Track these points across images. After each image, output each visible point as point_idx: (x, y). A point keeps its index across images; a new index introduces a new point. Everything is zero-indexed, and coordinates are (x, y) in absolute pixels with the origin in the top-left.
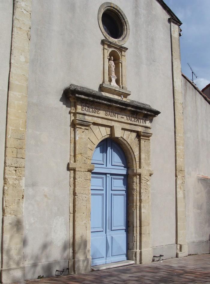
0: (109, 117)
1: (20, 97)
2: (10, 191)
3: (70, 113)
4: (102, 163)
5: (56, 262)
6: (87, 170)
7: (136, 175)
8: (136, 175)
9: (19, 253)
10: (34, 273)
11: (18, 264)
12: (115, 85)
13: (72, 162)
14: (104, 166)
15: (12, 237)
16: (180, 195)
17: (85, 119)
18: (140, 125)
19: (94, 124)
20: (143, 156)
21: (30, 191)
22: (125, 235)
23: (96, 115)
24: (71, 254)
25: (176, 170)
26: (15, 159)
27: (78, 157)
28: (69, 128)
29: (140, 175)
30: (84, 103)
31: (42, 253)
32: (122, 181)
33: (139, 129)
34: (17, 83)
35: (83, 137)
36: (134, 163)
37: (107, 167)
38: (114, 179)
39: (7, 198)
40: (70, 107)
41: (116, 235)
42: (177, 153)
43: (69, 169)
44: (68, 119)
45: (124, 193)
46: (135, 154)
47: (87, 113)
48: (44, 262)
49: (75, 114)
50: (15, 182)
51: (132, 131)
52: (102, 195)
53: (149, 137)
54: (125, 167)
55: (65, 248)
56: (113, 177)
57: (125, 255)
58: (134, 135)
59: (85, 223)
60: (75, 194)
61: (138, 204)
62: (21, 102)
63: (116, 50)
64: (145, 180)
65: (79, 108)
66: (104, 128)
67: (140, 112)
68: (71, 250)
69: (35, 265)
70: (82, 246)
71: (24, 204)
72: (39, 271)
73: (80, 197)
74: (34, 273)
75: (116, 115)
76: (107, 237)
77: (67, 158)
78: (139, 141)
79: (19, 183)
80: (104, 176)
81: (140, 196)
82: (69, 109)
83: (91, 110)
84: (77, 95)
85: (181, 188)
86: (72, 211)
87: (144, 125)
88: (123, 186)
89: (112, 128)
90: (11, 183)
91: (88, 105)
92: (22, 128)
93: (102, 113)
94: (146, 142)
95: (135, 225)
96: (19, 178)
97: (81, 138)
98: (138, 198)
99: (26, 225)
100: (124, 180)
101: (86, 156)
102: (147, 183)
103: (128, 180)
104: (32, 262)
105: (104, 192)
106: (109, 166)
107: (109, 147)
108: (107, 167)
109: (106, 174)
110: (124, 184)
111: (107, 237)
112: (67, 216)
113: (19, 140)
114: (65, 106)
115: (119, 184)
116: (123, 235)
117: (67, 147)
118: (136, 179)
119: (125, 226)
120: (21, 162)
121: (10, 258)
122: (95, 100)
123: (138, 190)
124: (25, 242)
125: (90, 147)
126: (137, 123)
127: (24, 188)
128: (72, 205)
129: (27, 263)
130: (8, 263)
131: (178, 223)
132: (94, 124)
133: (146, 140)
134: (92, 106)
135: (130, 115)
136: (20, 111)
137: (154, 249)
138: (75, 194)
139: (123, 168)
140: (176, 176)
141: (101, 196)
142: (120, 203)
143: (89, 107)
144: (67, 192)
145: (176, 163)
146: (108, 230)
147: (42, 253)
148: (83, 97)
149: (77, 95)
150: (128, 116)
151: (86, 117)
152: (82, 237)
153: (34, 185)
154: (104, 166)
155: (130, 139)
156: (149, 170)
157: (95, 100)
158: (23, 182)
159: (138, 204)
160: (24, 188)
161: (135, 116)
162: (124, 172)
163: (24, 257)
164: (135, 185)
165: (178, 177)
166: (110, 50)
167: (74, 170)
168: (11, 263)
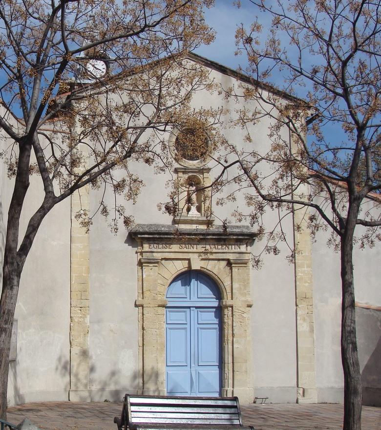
0: (186, 250)
3: (137, 253)
4: (185, 296)
5: (125, 389)
6: (157, 306)
7: (227, 307)
8: (227, 307)
9: (86, 377)
10: (101, 396)
11: (86, 386)
12: (196, 212)
13: (140, 299)
14: (188, 299)
15: (79, 364)
16: (303, 327)
17: (153, 256)
18: (231, 252)
21: (96, 327)
23: (168, 250)
24: (141, 384)
25: (296, 298)
26: (79, 301)
27: (147, 294)
28: (136, 268)
29: (232, 307)
30: (150, 241)
31: (111, 379)
32: (213, 314)
33: (231, 257)
36: (225, 294)
37: (191, 300)
39: (73, 333)
40: (137, 247)
42: (298, 277)
43: (136, 306)
44: (136, 258)
45: (217, 326)
46: (225, 284)
48: (112, 387)
49: (141, 253)
50: (80, 320)
51: (219, 260)
52: (185, 329)
53: (246, 263)
54: (217, 299)
55: (135, 377)
56: (199, 310)
57: (218, 393)
58: (224, 263)
59: (155, 356)
60: (143, 329)
61: (230, 339)
62: (83, 252)
63: (195, 174)
64: (240, 311)
65: (146, 247)
67: (227, 238)
68: (141, 381)
69: (103, 389)
70: (153, 377)
71: (89, 339)
72: (106, 396)
73: (149, 332)
74: (101, 396)
76: (191, 375)
77: (135, 296)
78: (231, 269)
79: (84, 320)
80: (188, 310)
81: (233, 331)
82: (136, 249)
83: (161, 246)
84: (139, 236)
86: (141, 345)
87: (238, 250)
88: (215, 319)
89: (189, 260)
90: (76, 320)
91: (156, 242)
92: (85, 274)
93: (175, 247)
94: (240, 270)
95: (226, 362)
96: (84, 316)
97: (148, 276)
98: (230, 332)
101: (155, 292)
102: (243, 315)
103: (219, 311)
104: (99, 387)
105: (188, 326)
107: (193, 280)
108: (191, 300)
109: (189, 307)
110: (216, 317)
111: (191, 375)
112: (136, 349)
115: (210, 317)
116: (216, 371)
117: (135, 285)
118: (227, 311)
119: (218, 362)
120: (85, 303)
123: (230, 323)
124: (92, 369)
125: (162, 283)
126: (226, 250)
127: (88, 324)
129: (95, 387)
131: (299, 363)
133: (239, 268)
134: (162, 242)
136: (82, 260)
138: (143, 329)
139: (215, 300)
140: (297, 305)
144: (137, 326)
145: (296, 289)
146: (193, 365)
147: (111, 379)
148: (146, 236)
149: (139, 236)
150: (212, 245)
151: (155, 254)
153: (99, 321)
154: (188, 299)
155: (217, 269)
156: (247, 301)
157: (162, 236)
158: (88, 320)
159: (230, 339)
160: (88, 324)
161: (222, 243)
162: (216, 304)
163: (91, 381)
164: (227, 318)
165: (300, 306)
166: (186, 176)
167: (142, 306)
168: (79, 384)
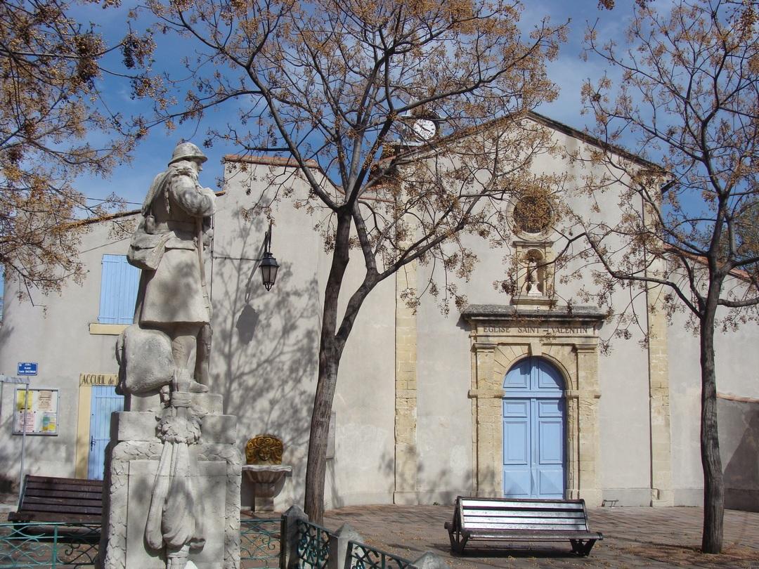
1: (408, 330)
2: (401, 420)
3: (470, 337)
7: (572, 398)
8: (572, 398)
9: (413, 477)
10: (430, 498)
11: (413, 487)
15: (405, 463)
16: (658, 421)
17: (488, 341)
18: (577, 336)
19: (503, 344)
20: (581, 374)
22: (562, 471)
23: (505, 334)
27: (481, 383)
28: (469, 354)
29: (578, 398)
33: (577, 341)
34: (404, 317)
35: (487, 361)
38: (507, 403)
39: (398, 427)
41: (545, 470)
42: (652, 365)
43: (469, 397)
44: (469, 343)
45: (560, 420)
46: (570, 372)
47: (491, 334)
49: (475, 337)
52: (525, 422)
55: (468, 477)
56: (505, 401)
61: (576, 434)
65: (481, 330)
66: (519, 347)
69: (432, 491)
70: (489, 478)
71: (416, 433)
72: (436, 498)
74: (430, 498)
75: (536, 329)
77: (468, 385)
78: (577, 355)
80: (528, 401)
82: (469, 333)
83: (497, 329)
84: (473, 318)
85: (659, 413)
86: (475, 441)
87: (585, 334)
89: (529, 345)
90: (402, 413)
91: (492, 325)
94: (586, 357)
95: (571, 459)
96: (411, 408)
97: (482, 363)
98: (576, 426)
99: (419, 449)
100: (559, 404)
103: (564, 403)
104: (427, 488)
105: (528, 420)
106: (534, 388)
109: (529, 399)
110: (559, 409)
112: (469, 445)
113: (409, 373)
114: (463, 330)
115: (553, 409)
117: (468, 373)
121: (404, 480)
122: (499, 318)
123: (576, 416)
124: (420, 468)
126: (571, 334)
128: (475, 434)
129: (423, 488)
130: (401, 486)
132: (503, 344)
135: (559, 326)
136: (409, 345)
137: (605, 491)
141: (523, 425)
142: (553, 432)
143: (494, 327)
144: (469, 421)
145: (649, 378)
146: (533, 463)
147: (440, 479)
148: (481, 318)
149: (473, 318)
151: (490, 339)
152: (488, 467)
153: (428, 414)
155: (560, 355)
156: (594, 391)
157: (499, 318)
159: (576, 434)
160: (416, 417)
162: (560, 395)
163: (419, 482)
166: (526, 251)
167: (476, 397)
